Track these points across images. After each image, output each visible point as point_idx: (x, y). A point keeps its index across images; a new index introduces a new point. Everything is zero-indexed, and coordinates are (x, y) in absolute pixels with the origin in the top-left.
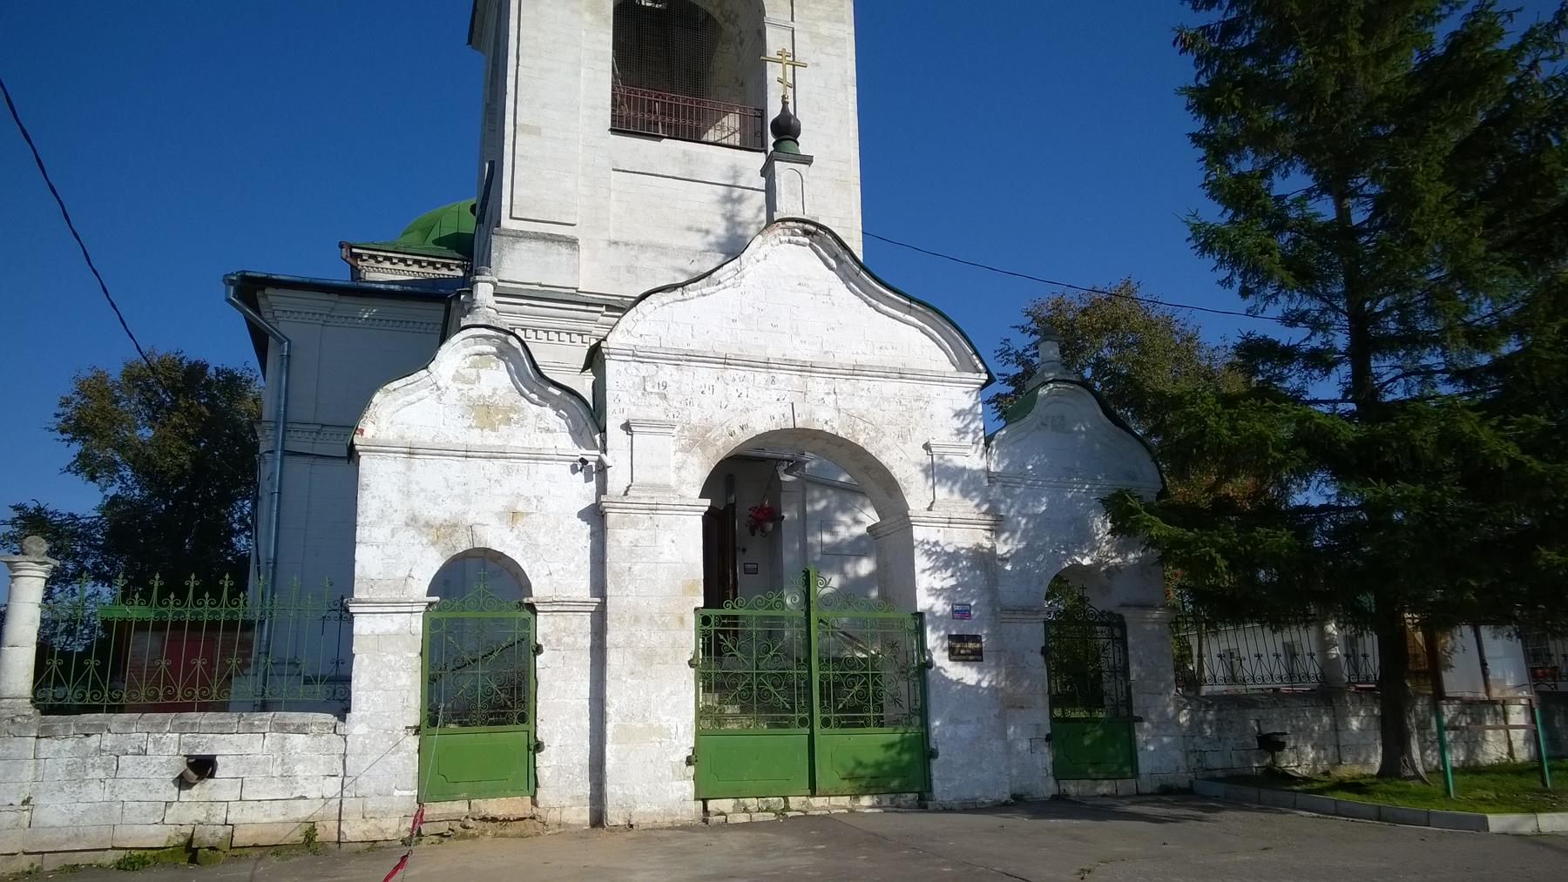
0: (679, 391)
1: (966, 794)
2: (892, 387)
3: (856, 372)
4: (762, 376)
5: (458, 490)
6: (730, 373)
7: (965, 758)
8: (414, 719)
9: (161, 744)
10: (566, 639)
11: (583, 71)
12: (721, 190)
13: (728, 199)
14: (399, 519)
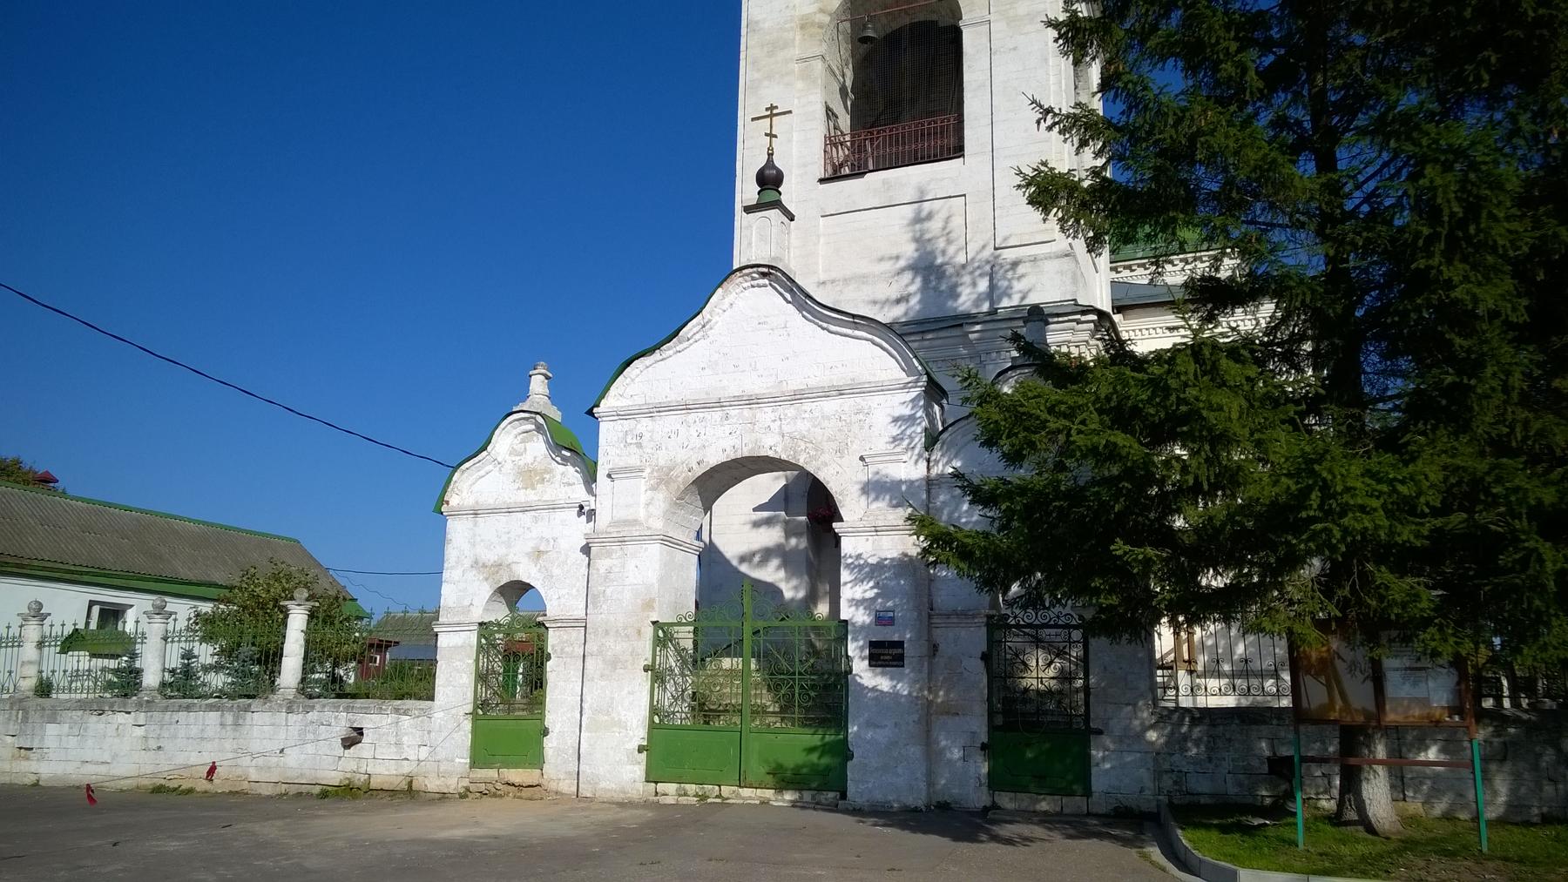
0: (652, 440)
1: (879, 796)
2: (831, 405)
3: (798, 397)
4: (717, 415)
5: (504, 538)
6: (693, 416)
7: (880, 760)
8: (470, 708)
9: (335, 718)
11: (795, 135)
12: (909, 212)
13: (918, 220)
14: (467, 563)
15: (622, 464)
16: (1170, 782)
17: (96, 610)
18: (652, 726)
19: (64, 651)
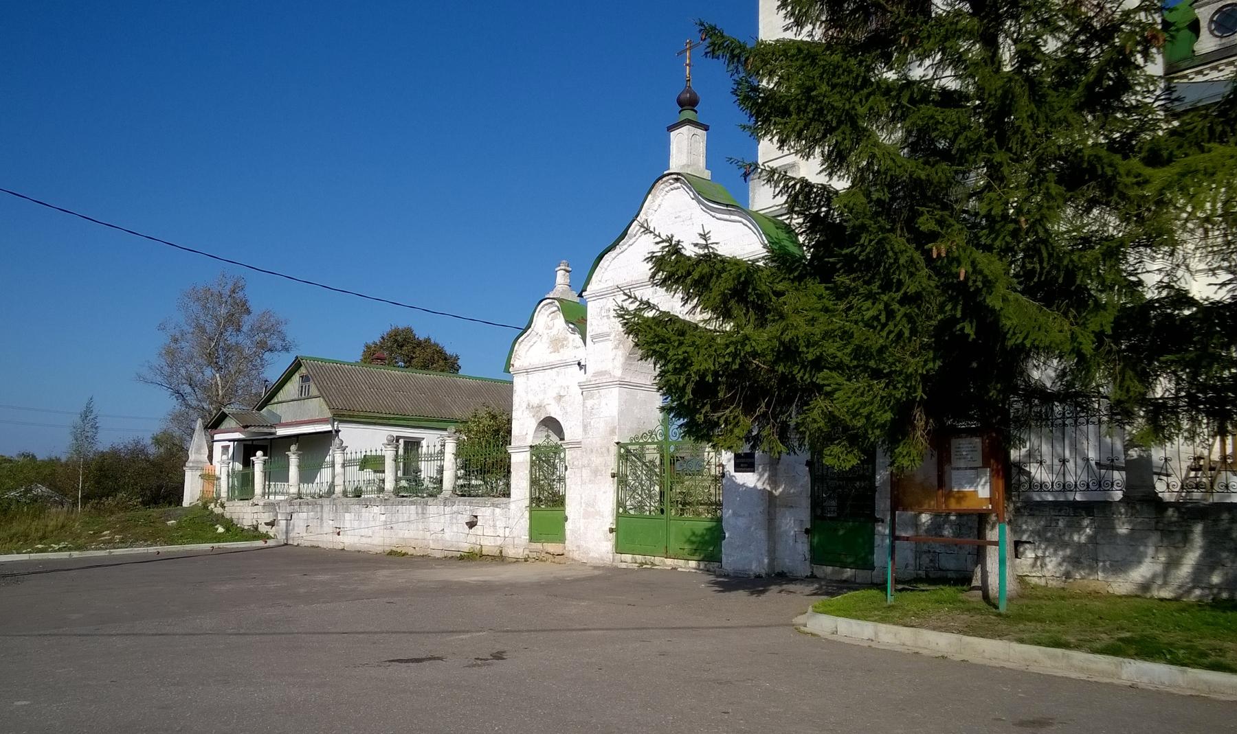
8: (527, 502)
9: (465, 509)
14: (525, 405)
15: (599, 331)
16: (928, 560)
17: (401, 441)
18: (618, 515)
19: (362, 469)
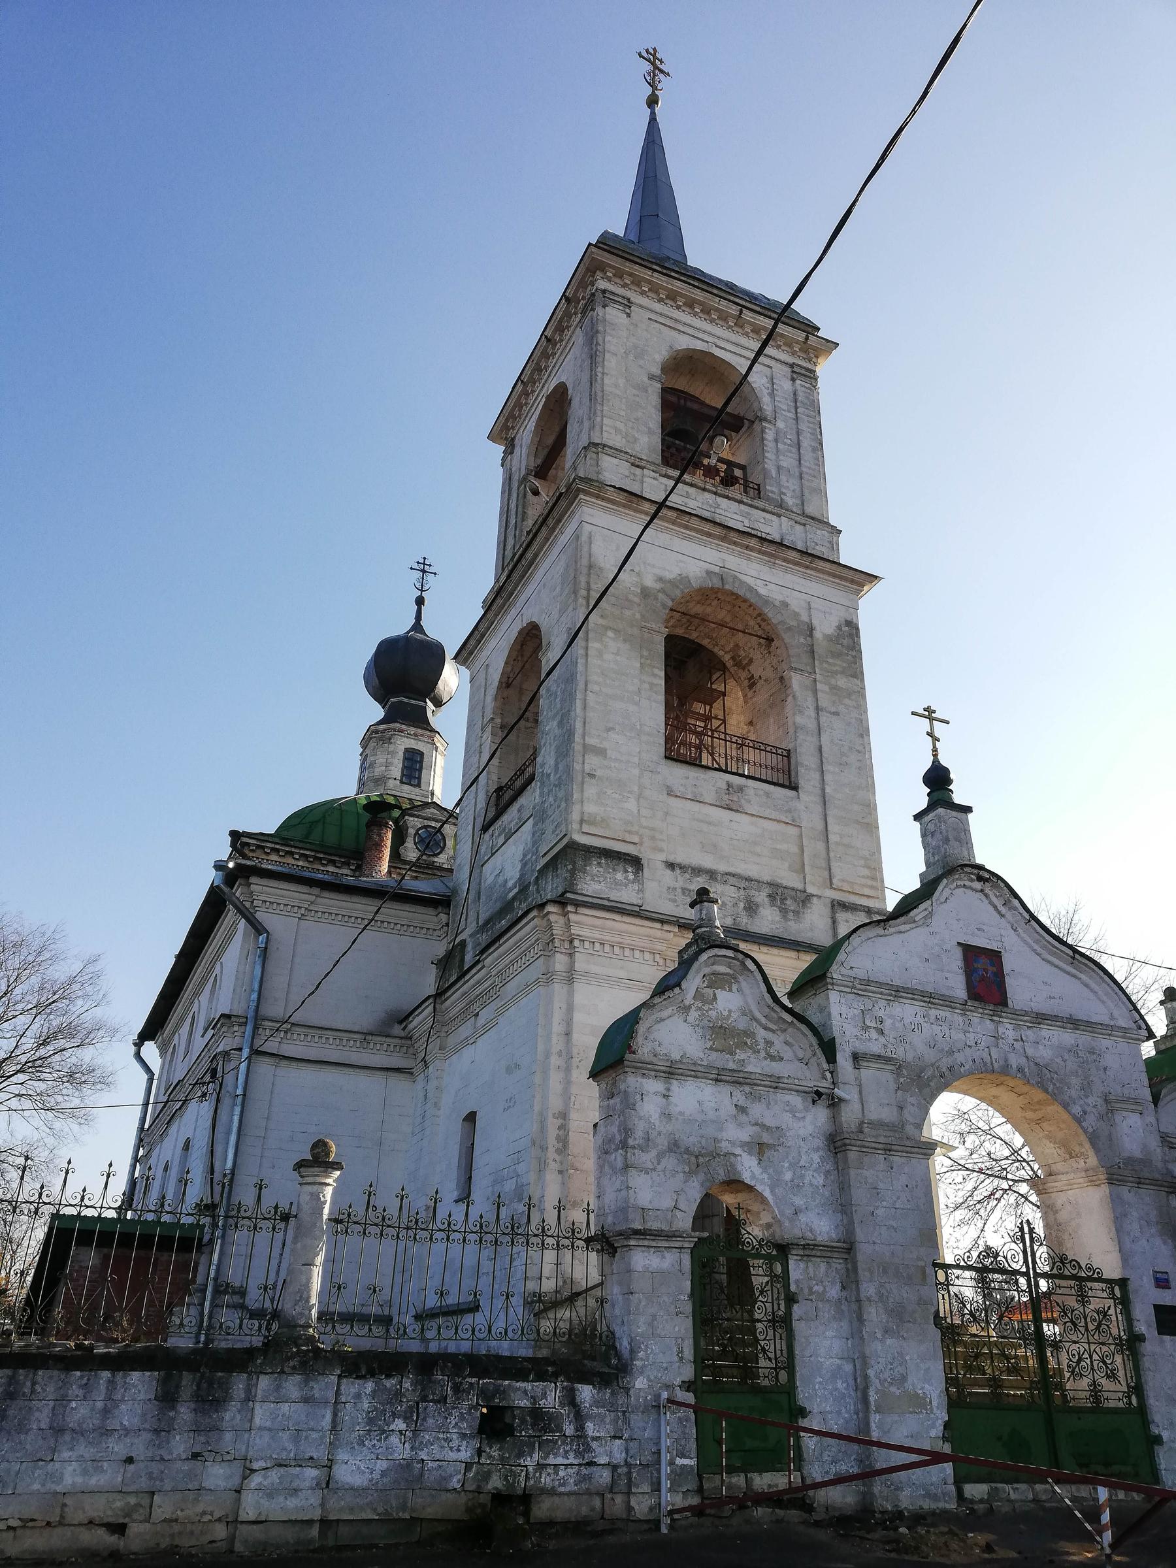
10: (816, 1288)
14: (662, 1142)
